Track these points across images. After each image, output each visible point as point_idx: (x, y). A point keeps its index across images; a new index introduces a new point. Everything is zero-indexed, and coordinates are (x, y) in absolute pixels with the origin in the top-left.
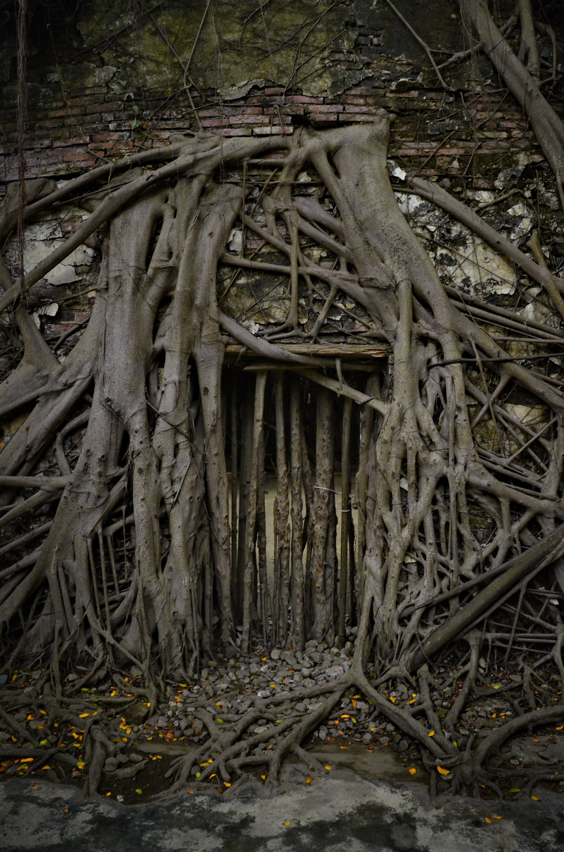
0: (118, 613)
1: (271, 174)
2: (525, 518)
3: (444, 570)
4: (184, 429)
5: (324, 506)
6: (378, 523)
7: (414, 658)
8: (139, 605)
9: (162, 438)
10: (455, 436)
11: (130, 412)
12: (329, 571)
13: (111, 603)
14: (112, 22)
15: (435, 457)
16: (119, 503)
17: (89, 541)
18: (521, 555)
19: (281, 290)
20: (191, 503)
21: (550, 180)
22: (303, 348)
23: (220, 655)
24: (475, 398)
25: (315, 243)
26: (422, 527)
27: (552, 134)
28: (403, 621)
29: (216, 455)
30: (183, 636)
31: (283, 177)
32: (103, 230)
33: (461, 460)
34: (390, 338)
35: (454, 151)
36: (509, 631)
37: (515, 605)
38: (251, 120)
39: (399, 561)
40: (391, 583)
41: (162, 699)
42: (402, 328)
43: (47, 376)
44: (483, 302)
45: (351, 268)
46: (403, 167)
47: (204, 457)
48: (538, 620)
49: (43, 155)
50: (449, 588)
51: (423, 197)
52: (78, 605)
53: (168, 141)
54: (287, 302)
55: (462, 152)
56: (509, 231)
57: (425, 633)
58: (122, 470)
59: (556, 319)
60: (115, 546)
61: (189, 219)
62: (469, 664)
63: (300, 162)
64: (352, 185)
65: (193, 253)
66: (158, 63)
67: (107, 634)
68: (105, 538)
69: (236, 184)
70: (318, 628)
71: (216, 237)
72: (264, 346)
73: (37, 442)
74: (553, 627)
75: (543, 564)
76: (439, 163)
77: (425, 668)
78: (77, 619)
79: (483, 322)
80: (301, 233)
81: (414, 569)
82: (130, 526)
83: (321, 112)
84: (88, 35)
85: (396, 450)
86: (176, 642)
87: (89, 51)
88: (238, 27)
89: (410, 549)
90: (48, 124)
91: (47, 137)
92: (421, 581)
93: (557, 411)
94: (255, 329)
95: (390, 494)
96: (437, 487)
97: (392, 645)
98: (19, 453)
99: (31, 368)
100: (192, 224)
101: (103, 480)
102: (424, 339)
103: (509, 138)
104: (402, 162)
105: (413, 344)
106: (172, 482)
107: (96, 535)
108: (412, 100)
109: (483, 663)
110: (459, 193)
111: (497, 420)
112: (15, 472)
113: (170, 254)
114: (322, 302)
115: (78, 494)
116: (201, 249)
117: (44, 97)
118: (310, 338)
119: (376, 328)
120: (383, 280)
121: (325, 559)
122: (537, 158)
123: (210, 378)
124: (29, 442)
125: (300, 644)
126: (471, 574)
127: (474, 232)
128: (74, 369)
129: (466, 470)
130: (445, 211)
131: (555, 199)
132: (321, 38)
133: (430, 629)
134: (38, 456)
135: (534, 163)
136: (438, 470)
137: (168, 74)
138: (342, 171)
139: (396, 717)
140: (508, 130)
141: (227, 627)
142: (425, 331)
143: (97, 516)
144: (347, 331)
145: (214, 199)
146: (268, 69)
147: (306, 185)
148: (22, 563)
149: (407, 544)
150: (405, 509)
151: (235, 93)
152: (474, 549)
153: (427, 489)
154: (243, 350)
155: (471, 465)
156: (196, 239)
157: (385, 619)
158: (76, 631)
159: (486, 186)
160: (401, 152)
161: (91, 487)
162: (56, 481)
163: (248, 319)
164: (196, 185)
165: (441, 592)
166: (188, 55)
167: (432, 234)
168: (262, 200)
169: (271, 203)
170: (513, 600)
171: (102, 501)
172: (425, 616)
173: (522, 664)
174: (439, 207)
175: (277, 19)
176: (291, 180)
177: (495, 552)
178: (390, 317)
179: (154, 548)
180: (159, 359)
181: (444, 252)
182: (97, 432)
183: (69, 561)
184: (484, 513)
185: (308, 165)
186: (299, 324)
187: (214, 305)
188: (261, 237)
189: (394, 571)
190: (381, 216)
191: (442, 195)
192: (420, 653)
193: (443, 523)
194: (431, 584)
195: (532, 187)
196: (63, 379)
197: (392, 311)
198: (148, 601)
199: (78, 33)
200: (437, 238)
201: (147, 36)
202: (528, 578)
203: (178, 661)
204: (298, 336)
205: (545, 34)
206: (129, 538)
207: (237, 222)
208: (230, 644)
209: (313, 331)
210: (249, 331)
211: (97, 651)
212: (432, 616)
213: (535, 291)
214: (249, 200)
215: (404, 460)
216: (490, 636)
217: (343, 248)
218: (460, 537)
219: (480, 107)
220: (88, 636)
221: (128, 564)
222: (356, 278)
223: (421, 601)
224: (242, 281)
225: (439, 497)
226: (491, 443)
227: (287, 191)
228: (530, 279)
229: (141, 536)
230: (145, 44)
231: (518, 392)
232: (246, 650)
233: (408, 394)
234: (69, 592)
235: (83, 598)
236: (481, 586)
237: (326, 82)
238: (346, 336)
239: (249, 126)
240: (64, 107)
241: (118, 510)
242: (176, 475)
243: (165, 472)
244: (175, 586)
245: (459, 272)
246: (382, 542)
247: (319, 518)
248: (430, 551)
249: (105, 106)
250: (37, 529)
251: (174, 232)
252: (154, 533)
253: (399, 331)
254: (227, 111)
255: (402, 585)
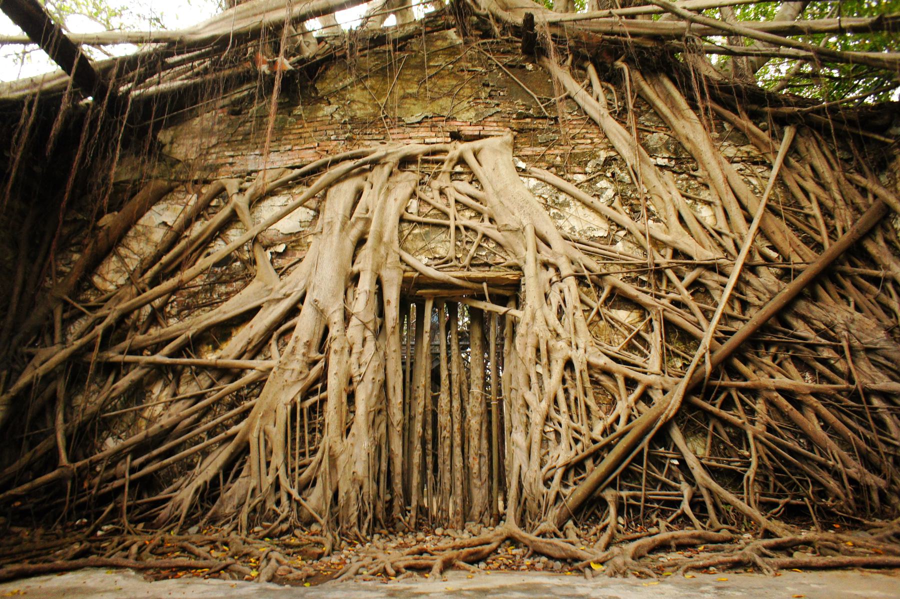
0: (307, 472)
1: (436, 166)
2: (638, 390)
3: (578, 436)
4: (371, 326)
5: (478, 405)
6: (521, 402)
7: (560, 513)
8: (325, 464)
9: (354, 331)
10: (575, 329)
11: (331, 310)
12: (483, 459)
13: (301, 467)
14: (337, 83)
15: (562, 344)
16: (316, 381)
17: (289, 407)
18: (639, 418)
19: (443, 236)
20: (374, 383)
21: (623, 166)
22: (460, 274)
23: (391, 529)
24: (587, 305)
25: (467, 207)
26: (556, 401)
27: (620, 137)
28: (547, 482)
29: (395, 351)
30: (360, 497)
31: (444, 167)
32: (322, 196)
33: (581, 345)
34: (521, 263)
35: (556, 152)
36: (640, 490)
37: (641, 464)
38: (424, 134)
39: (540, 428)
40: (535, 447)
41: (336, 547)
42: (530, 256)
43: (272, 289)
44: (585, 241)
45: (491, 220)
46: (524, 161)
47: (385, 353)
48: (663, 478)
49: (286, 154)
50: (583, 451)
51: (538, 179)
52: (273, 466)
53: (369, 146)
54: (448, 243)
55: (562, 152)
56: (599, 196)
57: (567, 492)
58: (321, 356)
59: (640, 251)
60: (310, 419)
61: (381, 188)
62: (609, 518)
63: (456, 158)
64: (490, 171)
65: (383, 209)
66: (364, 104)
67: (295, 493)
68: (302, 410)
69: (413, 172)
70: (476, 511)
71: (398, 202)
72: (432, 272)
73: (257, 336)
74: (678, 485)
75: (659, 424)
76: (547, 158)
77: (570, 523)
78: (270, 479)
79: (590, 254)
80: (457, 201)
81: (552, 436)
82: (324, 401)
83: (468, 130)
84: (321, 90)
85: (531, 341)
86: (353, 501)
87: (322, 98)
88: (416, 86)
89: (548, 419)
90: (291, 137)
91: (289, 144)
92: (559, 447)
93: (649, 309)
94: (425, 261)
95: (529, 377)
96: (565, 368)
97: (539, 506)
98: (244, 343)
99: (261, 284)
100: (383, 191)
101: (305, 359)
102: (546, 265)
103: (591, 143)
104: (524, 158)
105: (538, 271)
106: (360, 366)
107: (295, 404)
108: (527, 123)
109: (621, 520)
110: (562, 175)
111: (607, 320)
112: (239, 357)
113: (367, 211)
114: (472, 243)
115: (285, 370)
116: (388, 208)
117: (290, 122)
118: (464, 267)
119: (511, 260)
120: (514, 225)
121: (480, 448)
122: (613, 154)
123: (392, 294)
124: (251, 336)
125: (460, 523)
126: (600, 438)
127: (574, 197)
128: (293, 284)
129: (587, 351)
130: (554, 186)
131: (628, 177)
132: (467, 91)
133: (571, 489)
134: (258, 349)
135: (611, 157)
136: (565, 354)
137: (370, 110)
138: (483, 163)
139: (549, 546)
140: (591, 139)
141: (398, 503)
142: (545, 259)
143: (298, 387)
144: (491, 262)
145: (398, 179)
146: (435, 108)
147: (461, 173)
148: (231, 431)
149: (545, 413)
150: (541, 388)
151: (414, 119)
152: (600, 418)
153: (557, 368)
154: (416, 275)
155: (589, 349)
156: (385, 201)
157: (532, 480)
158: (267, 490)
159: (580, 171)
160: (521, 154)
161: (297, 365)
162: (268, 363)
163: (421, 254)
164: (387, 169)
165: (577, 454)
166: (384, 100)
167: (546, 200)
168: (430, 183)
169: (436, 184)
170: (638, 460)
171: (303, 376)
172: (565, 477)
173: (655, 520)
174: (550, 184)
175: (440, 82)
176: (450, 169)
177: (617, 420)
178: (520, 249)
179: (341, 417)
180: (355, 279)
181: (555, 211)
182: (305, 325)
183: (270, 428)
184: (605, 390)
185: (461, 161)
186: (456, 258)
187: (396, 243)
188: (429, 204)
189: (536, 437)
190: (510, 188)
191: (550, 176)
192: (564, 509)
193: (572, 398)
194: (568, 447)
195: (611, 171)
196: (283, 291)
197: (521, 245)
198: (333, 459)
199: (316, 89)
200: (550, 203)
201: (359, 90)
202: (649, 437)
203: (354, 519)
204: (456, 266)
205: (607, 88)
206: (321, 413)
207: (413, 195)
208: (400, 520)
209: (466, 262)
210: (421, 263)
211: (284, 510)
212: (572, 478)
213: (622, 233)
214: (421, 183)
215: (538, 350)
216: (625, 494)
217: (485, 208)
218: (587, 407)
219: (571, 126)
220: (277, 497)
221: (318, 435)
222: (496, 227)
223: (561, 461)
224: (416, 231)
225: (567, 376)
226: (603, 337)
227: (447, 176)
228: (618, 225)
229: (331, 407)
230: (357, 94)
231: (619, 299)
232: (413, 526)
233: (537, 298)
234: (266, 456)
235: (277, 460)
236: (609, 447)
237: (472, 114)
238: (490, 266)
239: (423, 138)
240: (303, 127)
241: (315, 387)
242: (363, 360)
243: (354, 356)
244: (356, 450)
245: (566, 223)
246: (525, 419)
247: (474, 415)
248: (564, 418)
249: (329, 127)
250: (247, 404)
251: (371, 197)
252: (342, 403)
253: (527, 257)
254: (408, 130)
255: (543, 451)
